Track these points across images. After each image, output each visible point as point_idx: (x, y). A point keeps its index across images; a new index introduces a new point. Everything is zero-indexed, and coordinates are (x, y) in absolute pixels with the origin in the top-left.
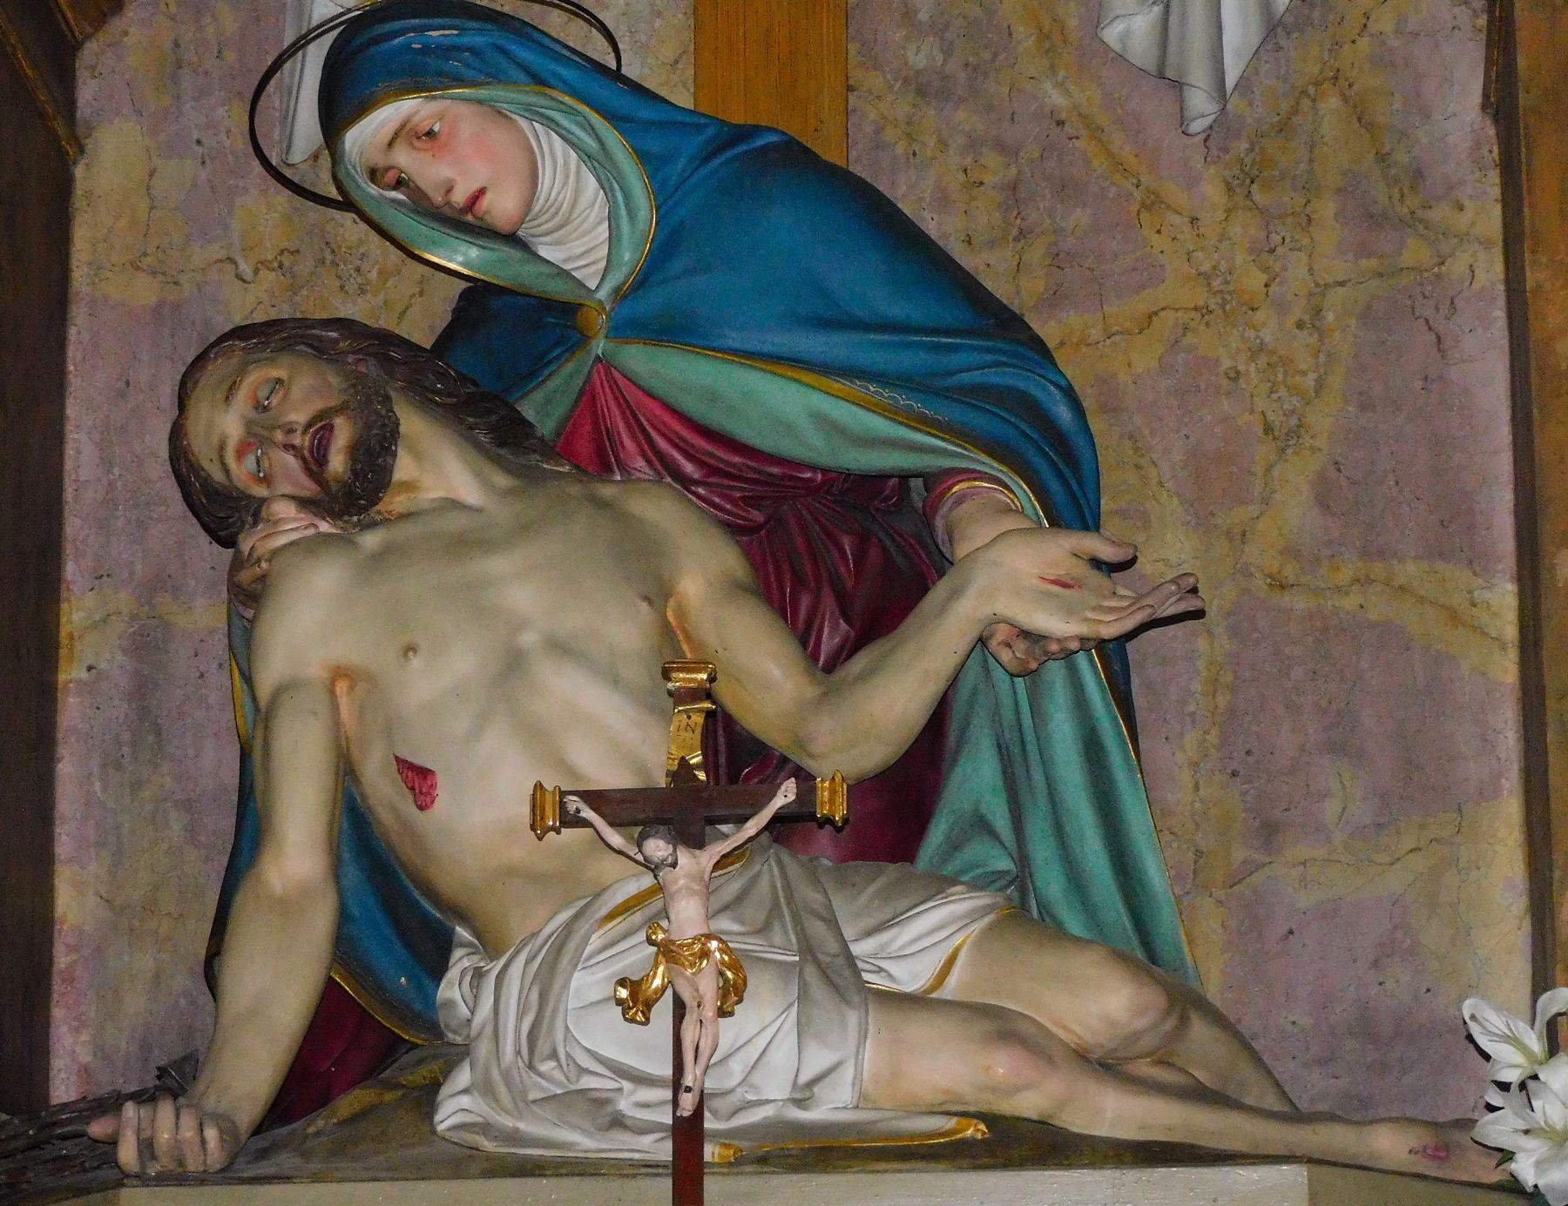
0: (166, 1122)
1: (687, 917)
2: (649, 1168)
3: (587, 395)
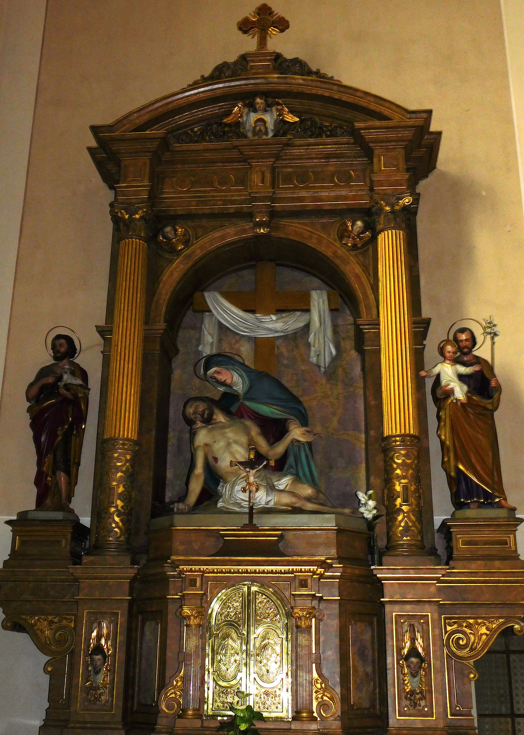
0: (181, 506)
1: (252, 479)
2: (245, 513)
3: (239, 407)
